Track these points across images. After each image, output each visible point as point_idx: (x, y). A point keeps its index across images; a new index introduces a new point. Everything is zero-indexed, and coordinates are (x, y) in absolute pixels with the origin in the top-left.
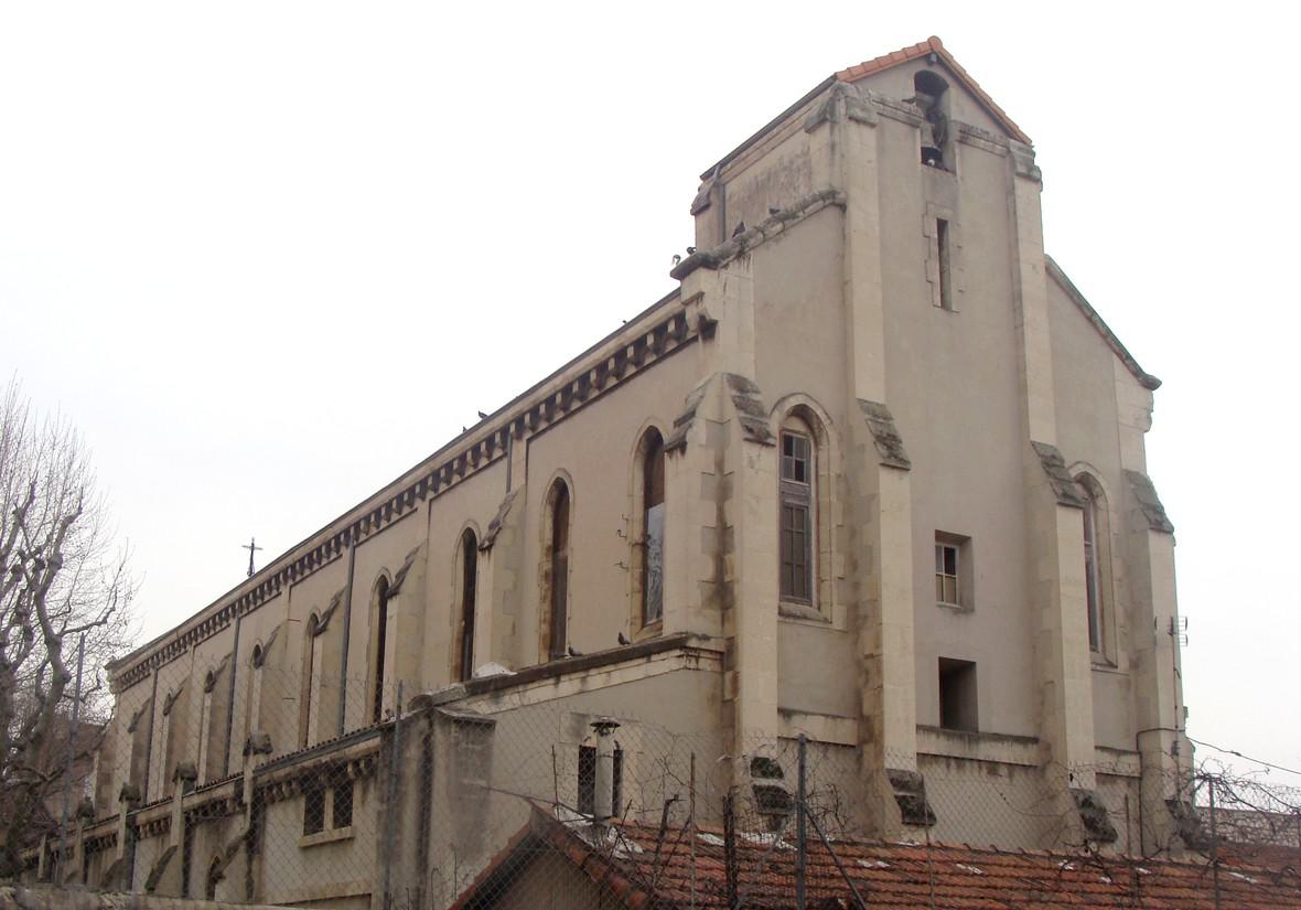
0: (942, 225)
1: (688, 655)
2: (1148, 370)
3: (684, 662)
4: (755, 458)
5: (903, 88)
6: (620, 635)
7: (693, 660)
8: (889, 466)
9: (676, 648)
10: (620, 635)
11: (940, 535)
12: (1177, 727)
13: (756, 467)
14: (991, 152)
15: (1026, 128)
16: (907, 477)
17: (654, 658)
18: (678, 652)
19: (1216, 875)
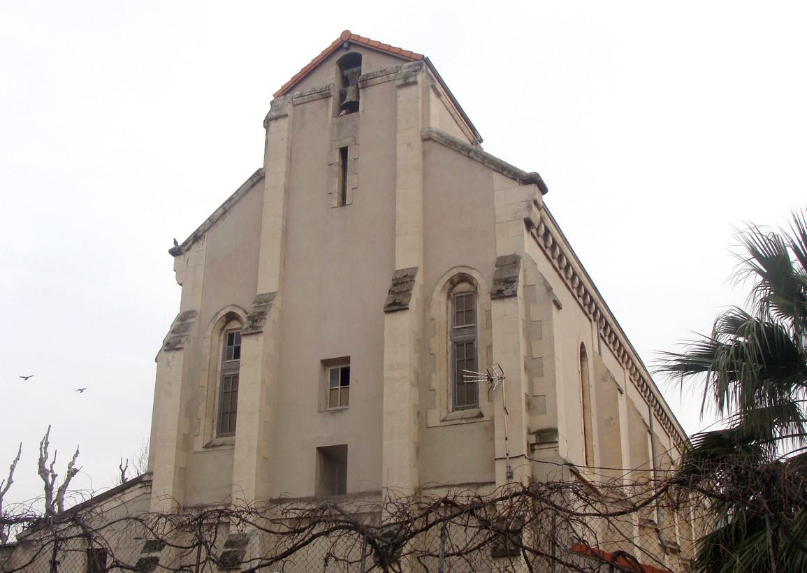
0: (344, 152)
1: (146, 486)
2: (527, 168)
3: (143, 490)
4: (170, 360)
5: (330, 76)
6: (582, 343)
7: (149, 487)
8: (247, 334)
9: (139, 483)
10: (582, 343)
11: (326, 363)
12: (507, 454)
13: (171, 364)
14: (389, 81)
15: (417, 49)
16: (261, 337)
17: (126, 491)
18: (139, 485)
19: (796, 435)
